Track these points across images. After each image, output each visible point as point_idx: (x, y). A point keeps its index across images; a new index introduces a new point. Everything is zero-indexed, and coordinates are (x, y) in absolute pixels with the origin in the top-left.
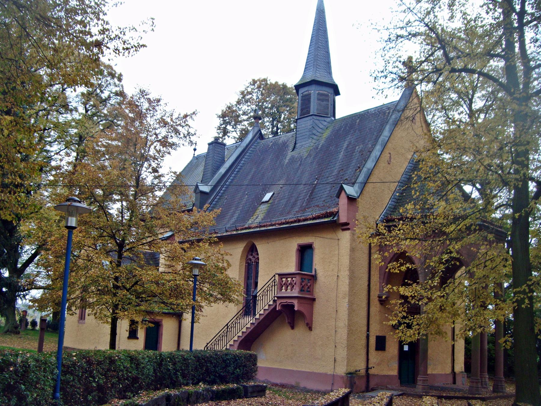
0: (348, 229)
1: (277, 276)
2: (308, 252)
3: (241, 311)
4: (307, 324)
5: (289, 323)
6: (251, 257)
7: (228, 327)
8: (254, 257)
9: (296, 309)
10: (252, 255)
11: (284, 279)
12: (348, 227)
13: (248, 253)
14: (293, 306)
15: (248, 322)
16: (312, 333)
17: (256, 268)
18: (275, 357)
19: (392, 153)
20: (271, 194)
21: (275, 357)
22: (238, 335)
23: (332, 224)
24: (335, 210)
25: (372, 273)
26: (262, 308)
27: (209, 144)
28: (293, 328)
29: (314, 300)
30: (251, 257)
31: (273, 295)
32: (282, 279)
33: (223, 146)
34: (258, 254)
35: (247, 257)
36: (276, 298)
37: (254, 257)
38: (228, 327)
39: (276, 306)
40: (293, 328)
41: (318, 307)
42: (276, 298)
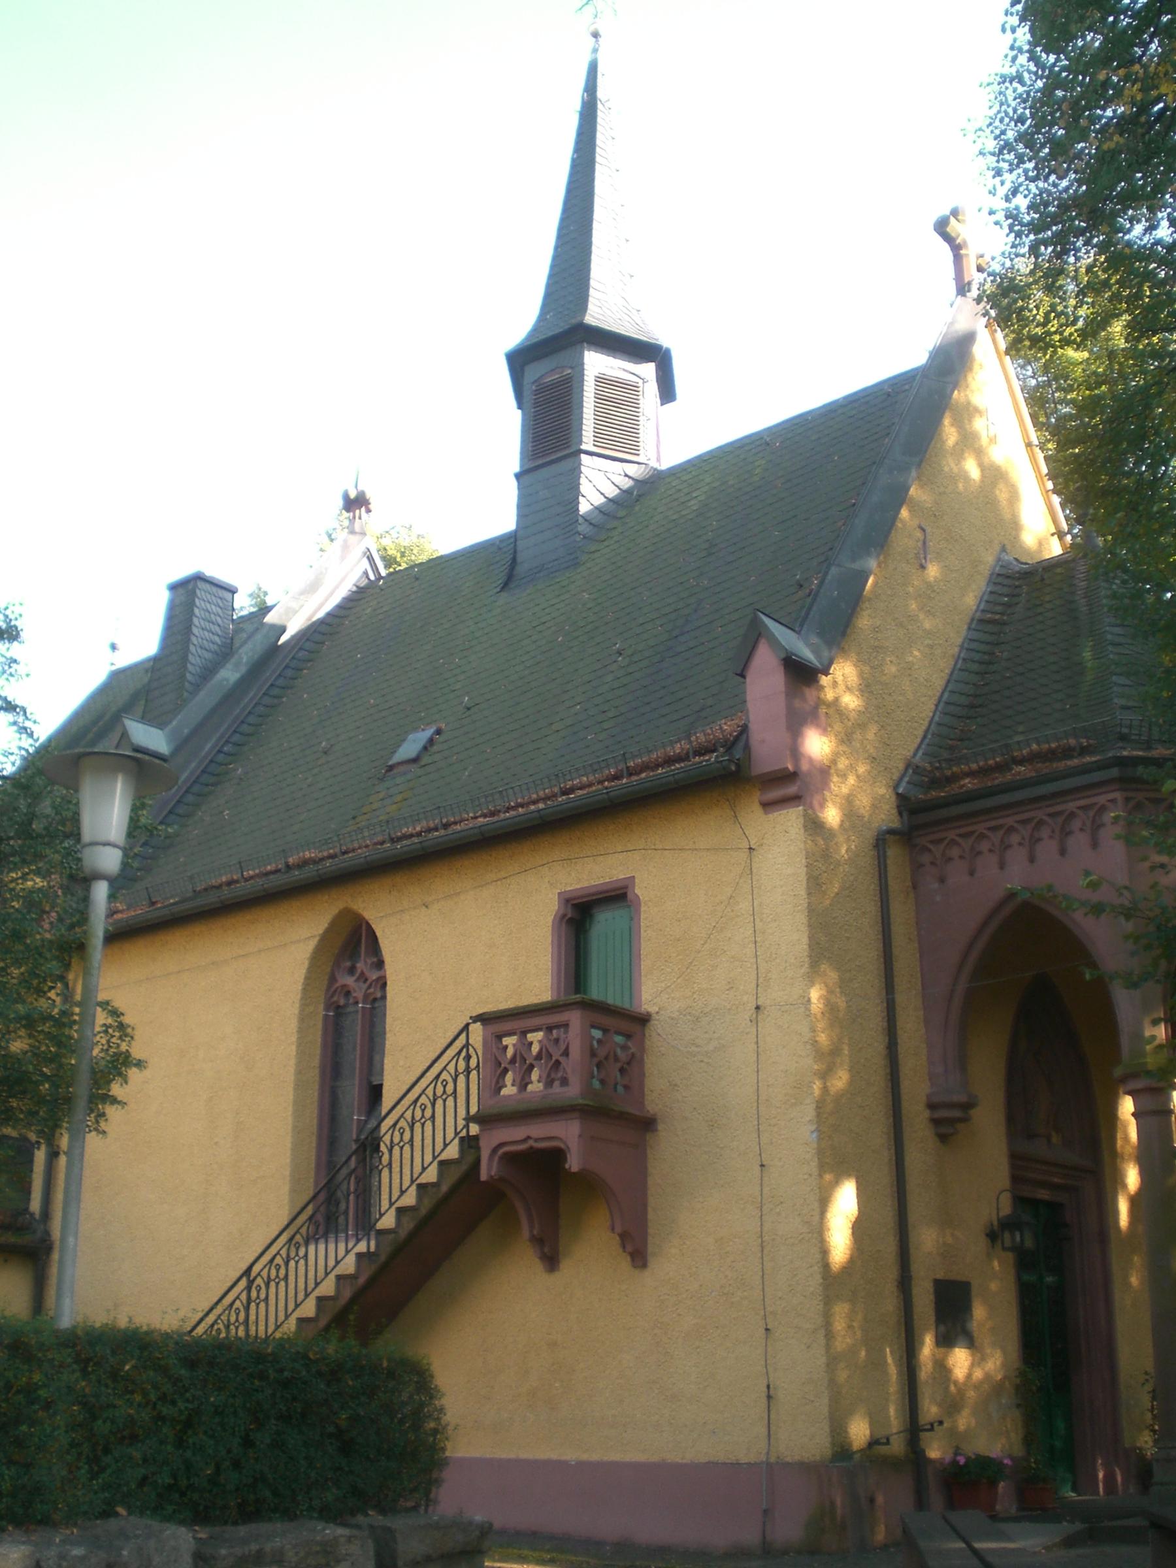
0: (796, 799)
1: (477, 1029)
2: (605, 921)
3: (310, 1210)
4: (624, 1237)
5: (538, 1241)
6: (350, 981)
7: (251, 1283)
8: (363, 978)
9: (574, 1163)
10: (352, 970)
11: (510, 1041)
12: (792, 790)
13: (337, 964)
14: (556, 1156)
15: (339, 1259)
16: (648, 1278)
17: (372, 1025)
18: (533, 1378)
19: (928, 530)
20: (423, 736)
21: (533, 1378)
22: (317, 1293)
23: (727, 776)
24: (728, 727)
25: (900, 998)
26: (410, 1168)
27: (173, 587)
28: (551, 1261)
29: (647, 1124)
30: (350, 981)
31: (462, 1113)
32: (499, 1037)
33: (228, 595)
34: (380, 964)
35: (333, 979)
36: (474, 1129)
37: (363, 978)
38: (251, 1283)
39: (477, 1162)
40: (551, 1261)
41: (665, 1153)
42: (474, 1129)
